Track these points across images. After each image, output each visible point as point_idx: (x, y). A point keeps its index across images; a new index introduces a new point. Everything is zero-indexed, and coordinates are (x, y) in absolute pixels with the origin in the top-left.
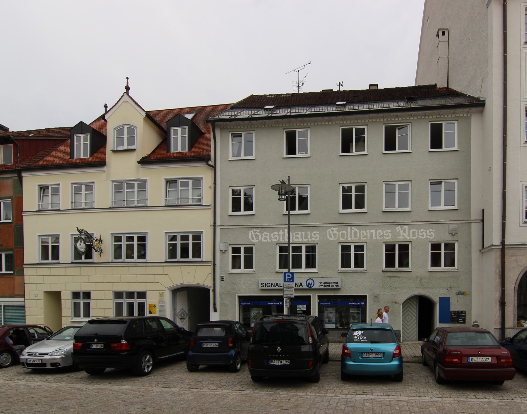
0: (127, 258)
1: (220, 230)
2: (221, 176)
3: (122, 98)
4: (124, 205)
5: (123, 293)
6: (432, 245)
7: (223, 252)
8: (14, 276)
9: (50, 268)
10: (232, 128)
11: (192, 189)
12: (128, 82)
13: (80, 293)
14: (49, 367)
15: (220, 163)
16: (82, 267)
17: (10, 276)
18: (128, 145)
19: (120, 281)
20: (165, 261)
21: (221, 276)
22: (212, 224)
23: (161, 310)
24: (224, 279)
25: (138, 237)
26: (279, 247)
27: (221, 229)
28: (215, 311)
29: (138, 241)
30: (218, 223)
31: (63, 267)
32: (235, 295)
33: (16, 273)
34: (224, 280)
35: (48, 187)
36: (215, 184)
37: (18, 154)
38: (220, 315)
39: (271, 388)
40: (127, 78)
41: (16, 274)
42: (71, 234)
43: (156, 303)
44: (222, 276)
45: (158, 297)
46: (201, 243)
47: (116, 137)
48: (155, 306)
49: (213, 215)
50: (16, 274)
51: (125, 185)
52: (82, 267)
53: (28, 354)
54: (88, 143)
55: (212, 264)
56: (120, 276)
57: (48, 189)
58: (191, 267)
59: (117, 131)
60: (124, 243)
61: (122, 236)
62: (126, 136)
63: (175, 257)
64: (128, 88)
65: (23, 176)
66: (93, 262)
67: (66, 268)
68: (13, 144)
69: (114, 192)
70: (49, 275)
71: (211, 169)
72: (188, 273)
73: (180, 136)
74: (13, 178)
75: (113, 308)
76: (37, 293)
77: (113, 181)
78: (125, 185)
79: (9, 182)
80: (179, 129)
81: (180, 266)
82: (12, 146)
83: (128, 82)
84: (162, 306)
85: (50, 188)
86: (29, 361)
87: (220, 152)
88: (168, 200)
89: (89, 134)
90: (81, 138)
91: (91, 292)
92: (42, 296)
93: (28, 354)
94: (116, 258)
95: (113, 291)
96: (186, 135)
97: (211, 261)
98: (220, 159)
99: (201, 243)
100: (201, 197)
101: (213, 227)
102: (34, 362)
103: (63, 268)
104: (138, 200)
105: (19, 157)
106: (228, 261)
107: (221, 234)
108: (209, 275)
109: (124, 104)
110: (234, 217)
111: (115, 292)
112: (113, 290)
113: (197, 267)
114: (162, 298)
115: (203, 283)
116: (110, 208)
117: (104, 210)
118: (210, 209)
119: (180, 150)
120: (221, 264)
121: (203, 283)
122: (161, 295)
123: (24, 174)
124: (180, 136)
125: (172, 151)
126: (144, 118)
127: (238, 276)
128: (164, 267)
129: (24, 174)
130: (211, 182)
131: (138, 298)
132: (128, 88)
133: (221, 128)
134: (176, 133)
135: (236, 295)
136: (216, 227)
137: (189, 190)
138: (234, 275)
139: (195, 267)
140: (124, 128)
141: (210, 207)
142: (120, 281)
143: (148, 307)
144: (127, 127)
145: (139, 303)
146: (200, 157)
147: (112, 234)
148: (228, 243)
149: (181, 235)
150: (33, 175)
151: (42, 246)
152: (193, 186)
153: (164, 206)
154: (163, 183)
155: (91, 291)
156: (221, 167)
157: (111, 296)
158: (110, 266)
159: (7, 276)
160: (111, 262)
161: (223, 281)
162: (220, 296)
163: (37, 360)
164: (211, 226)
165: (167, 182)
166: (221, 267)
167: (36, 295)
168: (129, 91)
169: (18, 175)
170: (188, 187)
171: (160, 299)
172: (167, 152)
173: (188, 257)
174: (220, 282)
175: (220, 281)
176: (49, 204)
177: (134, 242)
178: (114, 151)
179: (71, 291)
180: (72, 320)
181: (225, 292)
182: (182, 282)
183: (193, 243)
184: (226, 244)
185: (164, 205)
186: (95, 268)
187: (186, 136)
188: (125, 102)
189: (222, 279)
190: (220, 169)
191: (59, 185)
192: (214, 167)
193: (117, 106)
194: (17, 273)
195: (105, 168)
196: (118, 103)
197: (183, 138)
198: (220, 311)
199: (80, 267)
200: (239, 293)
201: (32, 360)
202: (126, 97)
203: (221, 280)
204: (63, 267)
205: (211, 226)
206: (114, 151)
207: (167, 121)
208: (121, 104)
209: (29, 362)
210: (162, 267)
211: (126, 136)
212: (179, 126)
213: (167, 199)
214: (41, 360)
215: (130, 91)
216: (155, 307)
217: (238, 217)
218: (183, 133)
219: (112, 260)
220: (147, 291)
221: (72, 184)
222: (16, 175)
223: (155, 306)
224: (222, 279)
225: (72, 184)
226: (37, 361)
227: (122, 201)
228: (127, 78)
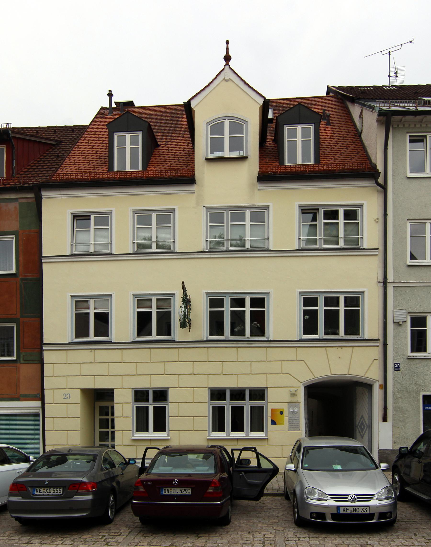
0: (233, 333)
1: (394, 290)
2: (394, 203)
3: (222, 73)
4: (227, 248)
5: (245, 390)
6: (413, 320)
7: (397, 324)
8: (18, 365)
9: (93, 351)
10: (407, 127)
11: (94, 229)
12: (227, 49)
13: (148, 391)
14: (329, 520)
15: (393, 181)
16: (96, 349)
17: (11, 364)
18: (231, 150)
19: (222, 371)
20: (299, 339)
21: (395, 364)
22: (381, 279)
23: (293, 418)
24: (400, 368)
25: (252, 300)
26: (411, 317)
27: (395, 288)
28: (385, 419)
29: (252, 306)
30: (390, 278)
31: (117, 349)
32: (418, 393)
33: (21, 359)
34: (400, 370)
35: (90, 216)
36: (385, 215)
37: (14, 161)
38: (393, 426)
39: (28, 534)
40: (227, 42)
41: (22, 361)
42: (70, 295)
43: (284, 407)
44: (397, 364)
45: (287, 398)
46: (171, 311)
47: (209, 137)
48: (282, 412)
49: (381, 265)
50: (22, 361)
51: (227, 216)
52: (96, 349)
53: (358, 498)
54: (139, 147)
55: (380, 344)
56: (222, 363)
57: (90, 219)
58: (344, 348)
59: (211, 126)
60: (321, 309)
61: (224, 299)
62: (227, 136)
63: (222, 334)
64: (227, 58)
65: (43, 197)
66: (174, 340)
67: (68, 351)
68: (5, 146)
69: (209, 227)
70: (91, 363)
71: (378, 191)
72: (340, 358)
73: (128, 146)
74: (20, 201)
75: (209, 416)
76: (67, 392)
77: (208, 209)
78: (227, 216)
79: (12, 206)
80: (299, 129)
81: (324, 347)
82: (3, 149)
83: (227, 49)
84: (294, 413)
85: (92, 217)
86: (344, 510)
87: (393, 164)
88: (75, 246)
89: (141, 132)
90: (297, 130)
91: (115, 390)
92: (77, 397)
93: (358, 498)
94: (306, 332)
95: (209, 388)
96: (310, 138)
97: (378, 340)
98: (393, 175)
99: (171, 311)
100: (360, 236)
101: (382, 284)
102: (354, 513)
103: (117, 350)
104: (94, 244)
105: (15, 167)
106: (406, 338)
107: (395, 296)
108: (375, 361)
109: (224, 83)
110: (417, 268)
111: (211, 390)
112: (209, 387)
113: (355, 348)
114: (294, 399)
115: (365, 375)
116: (203, 252)
117: (190, 255)
118: (376, 255)
119: (299, 162)
120: (394, 343)
121: (365, 375)
122: (293, 395)
123: (44, 194)
124: (128, 146)
125: (286, 163)
126: (259, 107)
127: (424, 363)
128: (298, 348)
129: (44, 194)
130: (378, 213)
131: (155, 400)
132: (227, 58)
133: (394, 126)
134: (293, 134)
135: (421, 393)
136: (388, 284)
137: (90, 232)
138: (417, 361)
139: (352, 348)
140: (224, 122)
141: (377, 252)
142: (222, 371)
143: (269, 414)
144: (230, 121)
145: (234, 409)
146: (136, 180)
147: (207, 294)
148: (406, 311)
149: (210, 299)
150: (179, 192)
151: (138, 313)
152: (157, 224)
153: (131, 254)
154: (69, 218)
155: (169, 388)
156: (394, 189)
157: (206, 395)
158: (205, 347)
159: (6, 365)
160: (205, 340)
161: (399, 372)
162: (393, 395)
163: (360, 508)
164: (379, 282)
165: (74, 217)
166: (395, 348)
167: (66, 396)
168: (230, 62)
169: (35, 195)
170: (244, 221)
171: (291, 401)
172: (108, 171)
173: (336, 332)
174: (393, 374)
175: (393, 372)
176: (91, 245)
177: (339, 306)
178: (209, 160)
179: (132, 388)
180: (133, 436)
181: (402, 389)
182: (328, 373)
183: (345, 310)
184: (404, 311)
185: (68, 253)
186: (177, 349)
187: (311, 140)
188: (226, 80)
189: (397, 368)
190: (393, 192)
191: (110, 212)
192: (384, 188)
193: (212, 86)
194: (23, 360)
195: (195, 187)
196: (215, 81)
197: (134, 151)
198: (394, 419)
199: (149, 348)
200: (425, 391)
201: (351, 509)
202: (227, 73)
203: (395, 370)
204: (117, 349)
205: (379, 282)
206: (209, 160)
207: (109, 123)
208: (218, 85)
209: (344, 513)
210: (295, 349)
211: (227, 136)
212: (128, 131)
213: (74, 244)
214: (368, 508)
215: (231, 63)
216: (282, 414)
217: (423, 268)
218: (134, 141)
219: (207, 338)
220: (267, 388)
221: (134, 211)
222: (33, 195)
223: (282, 413)
224: (397, 368)
225: (134, 211)
226: (361, 510)
227: (265, 239)
228: (227, 42)
